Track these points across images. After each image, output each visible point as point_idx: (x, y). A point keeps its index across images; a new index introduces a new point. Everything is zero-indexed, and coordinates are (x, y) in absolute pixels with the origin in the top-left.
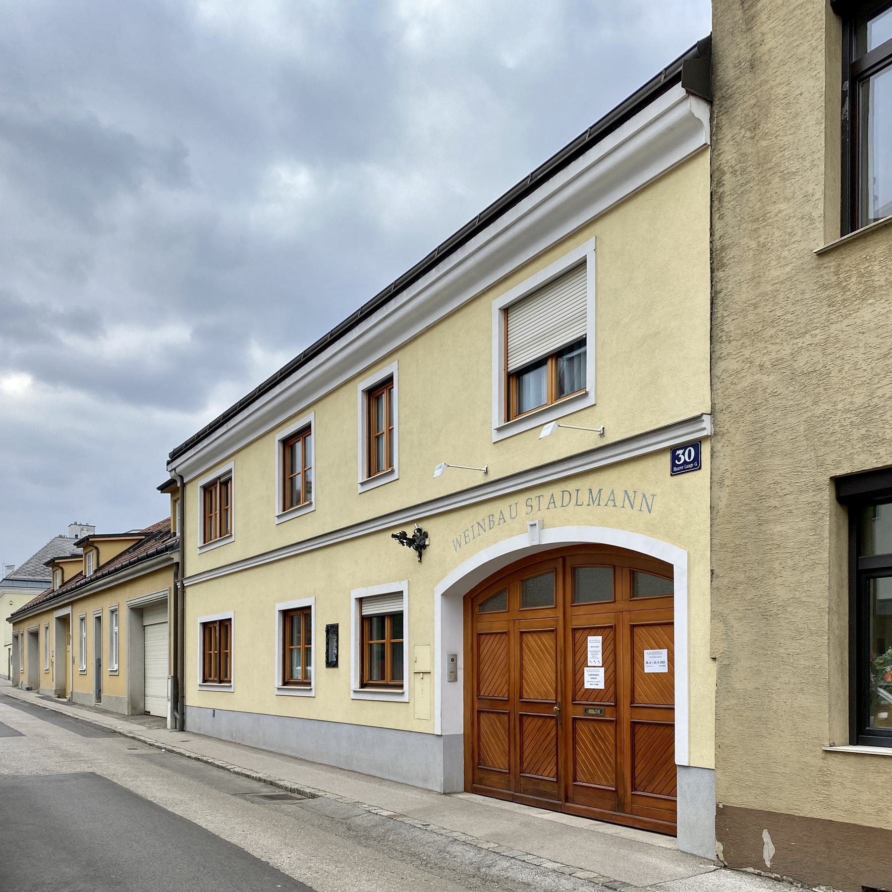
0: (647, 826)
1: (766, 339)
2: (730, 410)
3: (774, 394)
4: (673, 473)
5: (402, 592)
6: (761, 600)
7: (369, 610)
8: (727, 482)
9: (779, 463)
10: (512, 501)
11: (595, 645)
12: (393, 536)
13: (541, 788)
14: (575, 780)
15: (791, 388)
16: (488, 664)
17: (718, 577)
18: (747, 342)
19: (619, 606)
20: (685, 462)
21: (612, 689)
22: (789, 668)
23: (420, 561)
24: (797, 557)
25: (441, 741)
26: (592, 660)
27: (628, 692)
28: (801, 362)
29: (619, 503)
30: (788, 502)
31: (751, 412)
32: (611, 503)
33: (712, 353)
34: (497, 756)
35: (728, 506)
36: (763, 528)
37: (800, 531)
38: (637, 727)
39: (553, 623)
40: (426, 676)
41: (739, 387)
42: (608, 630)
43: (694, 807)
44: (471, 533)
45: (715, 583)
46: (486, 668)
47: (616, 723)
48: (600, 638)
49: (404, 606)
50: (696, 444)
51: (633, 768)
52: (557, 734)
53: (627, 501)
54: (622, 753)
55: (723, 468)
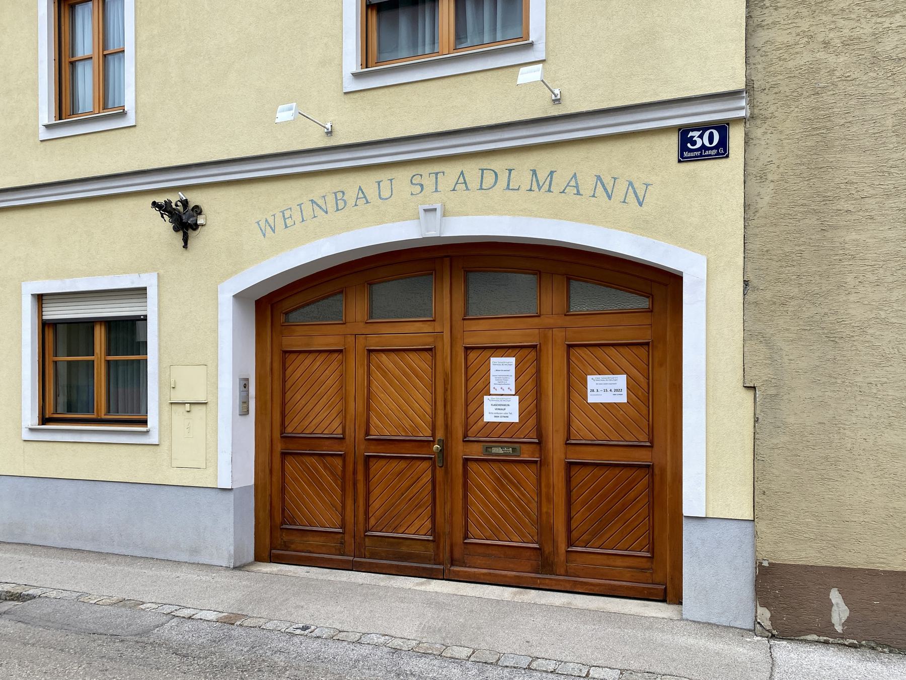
0: (596, 590)
1: (835, 12)
2: (776, 90)
3: (846, 79)
4: (682, 159)
5: (145, 289)
6: (826, 318)
7: (54, 313)
8: (770, 177)
9: (856, 159)
10: (384, 176)
11: (503, 371)
12: (154, 204)
13: (404, 549)
14: (466, 537)
15: (871, 74)
16: (302, 391)
17: (756, 289)
18: (805, 12)
19: (546, 321)
20: (704, 146)
21: (532, 422)
22: (870, 399)
23: (185, 246)
24: (881, 271)
25: (231, 496)
26: (497, 387)
27: (561, 426)
28: (889, 44)
29: (586, 190)
30: (867, 207)
31: (809, 97)
32: (571, 191)
33: (748, 17)
34: (319, 510)
35: (772, 205)
36: (829, 235)
37: (886, 240)
38: (574, 470)
39: (431, 340)
40: (198, 411)
41: (791, 64)
42: (526, 351)
43: (716, 571)
44: (297, 217)
45: (751, 297)
46: (298, 396)
47: (541, 464)
48: (513, 360)
49: (151, 309)
50: (723, 128)
51: (569, 519)
52: (434, 481)
53: (600, 188)
54: (549, 500)
55: (764, 159)
